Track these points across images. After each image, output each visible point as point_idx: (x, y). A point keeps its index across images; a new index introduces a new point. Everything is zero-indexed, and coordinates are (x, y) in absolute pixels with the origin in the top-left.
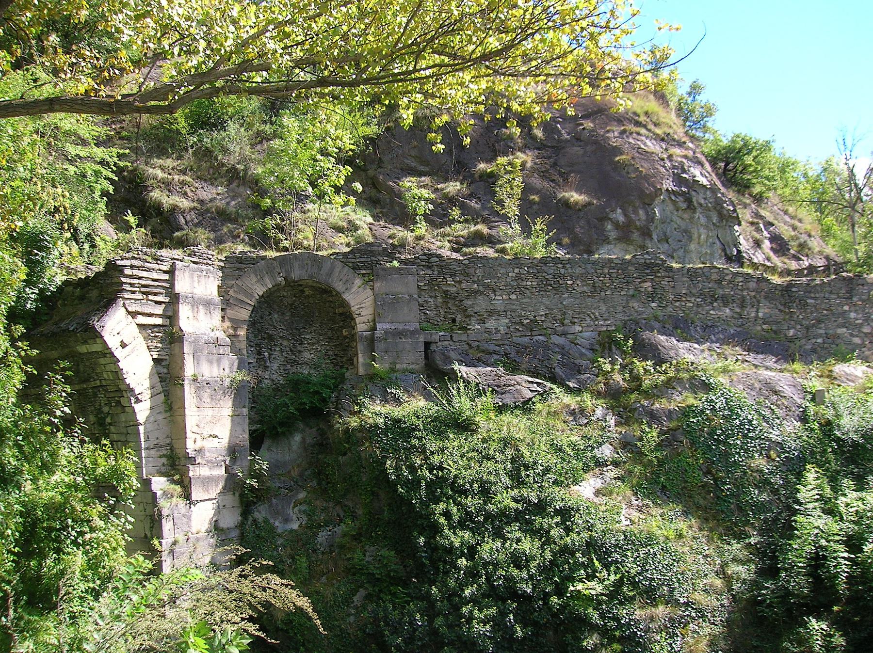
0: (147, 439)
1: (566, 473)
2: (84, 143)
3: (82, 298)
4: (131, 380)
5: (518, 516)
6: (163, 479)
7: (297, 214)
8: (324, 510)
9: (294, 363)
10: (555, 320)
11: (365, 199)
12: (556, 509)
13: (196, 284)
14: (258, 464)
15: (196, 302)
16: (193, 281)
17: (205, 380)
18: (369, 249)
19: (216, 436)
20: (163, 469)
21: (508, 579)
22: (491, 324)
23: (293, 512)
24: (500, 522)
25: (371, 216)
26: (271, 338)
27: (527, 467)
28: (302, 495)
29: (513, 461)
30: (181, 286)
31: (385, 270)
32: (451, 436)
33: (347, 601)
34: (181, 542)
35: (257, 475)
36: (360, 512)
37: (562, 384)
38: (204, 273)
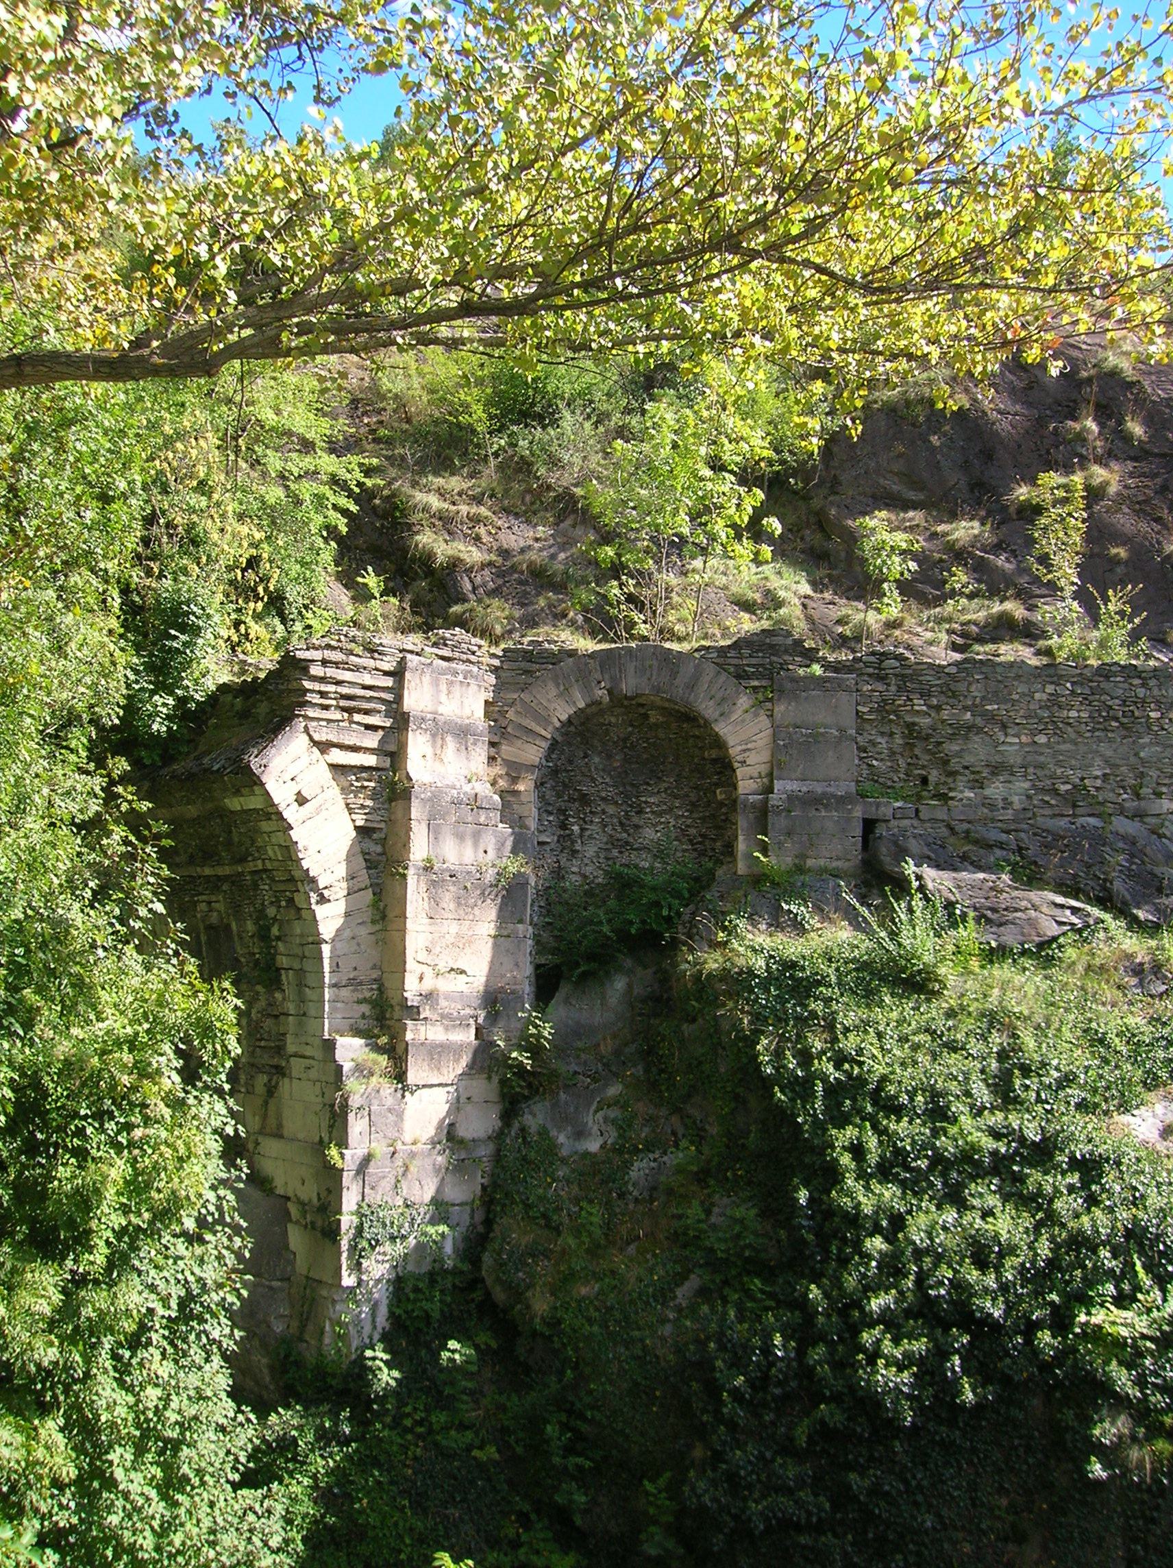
0: (336, 968)
1: (1108, 1088)
2: (307, 446)
3: (245, 715)
4: (310, 862)
5: (999, 1166)
6: (359, 1042)
7: (672, 579)
8: (651, 1120)
9: (625, 846)
10: (1123, 788)
11: (803, 552)
12: (1072, 1158)
13: (443, 698)
14: (536, 1026)
15: (440, 730)
16: (439, 691)
17: (448, 870)
19: (463, 972)
20: (362, 1024)
21: (958, 1285)
22: (995, 790)
23: (593, 1120)
24: (960, 1173)
25: (809, 582)
26: (584, 799)
27: (1026, 1071)
28: (614, 1090)
29: (1002, 1056)
30: (415, 699)
31: (796, 680)
32: (887, 999)
33: (664, 1294)
34: (378, 1156)
35: (535, 1050)
36: (714, 1130)
37: (1121, 911)
38: (461, 677)
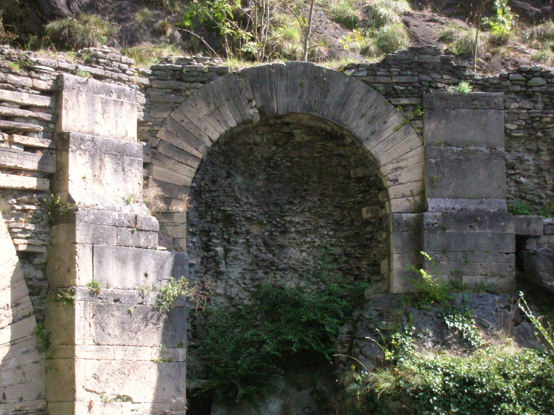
13: (99, 117)
16: (94, 111)
17: (112, 294)
18: (416, 59)
19: (129, 399)
31: (445, 98)
38: (114, 96)
